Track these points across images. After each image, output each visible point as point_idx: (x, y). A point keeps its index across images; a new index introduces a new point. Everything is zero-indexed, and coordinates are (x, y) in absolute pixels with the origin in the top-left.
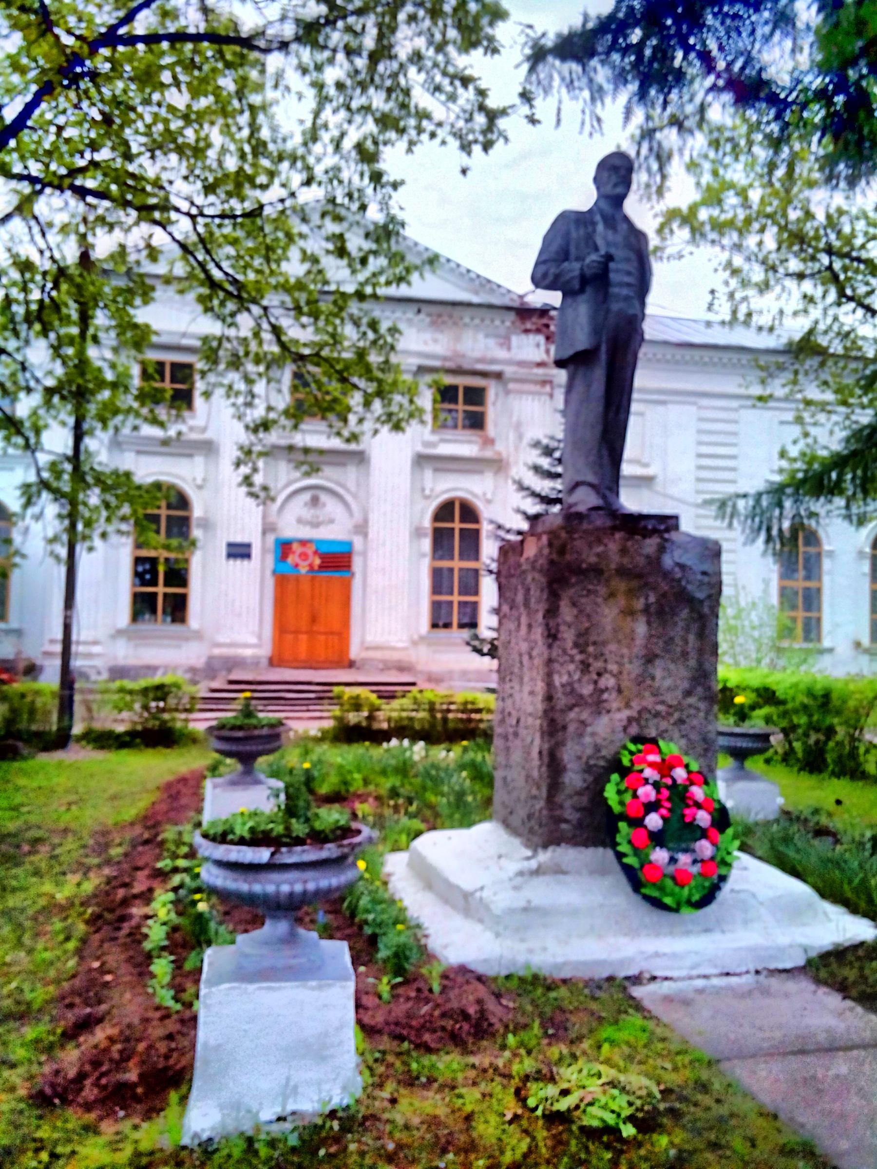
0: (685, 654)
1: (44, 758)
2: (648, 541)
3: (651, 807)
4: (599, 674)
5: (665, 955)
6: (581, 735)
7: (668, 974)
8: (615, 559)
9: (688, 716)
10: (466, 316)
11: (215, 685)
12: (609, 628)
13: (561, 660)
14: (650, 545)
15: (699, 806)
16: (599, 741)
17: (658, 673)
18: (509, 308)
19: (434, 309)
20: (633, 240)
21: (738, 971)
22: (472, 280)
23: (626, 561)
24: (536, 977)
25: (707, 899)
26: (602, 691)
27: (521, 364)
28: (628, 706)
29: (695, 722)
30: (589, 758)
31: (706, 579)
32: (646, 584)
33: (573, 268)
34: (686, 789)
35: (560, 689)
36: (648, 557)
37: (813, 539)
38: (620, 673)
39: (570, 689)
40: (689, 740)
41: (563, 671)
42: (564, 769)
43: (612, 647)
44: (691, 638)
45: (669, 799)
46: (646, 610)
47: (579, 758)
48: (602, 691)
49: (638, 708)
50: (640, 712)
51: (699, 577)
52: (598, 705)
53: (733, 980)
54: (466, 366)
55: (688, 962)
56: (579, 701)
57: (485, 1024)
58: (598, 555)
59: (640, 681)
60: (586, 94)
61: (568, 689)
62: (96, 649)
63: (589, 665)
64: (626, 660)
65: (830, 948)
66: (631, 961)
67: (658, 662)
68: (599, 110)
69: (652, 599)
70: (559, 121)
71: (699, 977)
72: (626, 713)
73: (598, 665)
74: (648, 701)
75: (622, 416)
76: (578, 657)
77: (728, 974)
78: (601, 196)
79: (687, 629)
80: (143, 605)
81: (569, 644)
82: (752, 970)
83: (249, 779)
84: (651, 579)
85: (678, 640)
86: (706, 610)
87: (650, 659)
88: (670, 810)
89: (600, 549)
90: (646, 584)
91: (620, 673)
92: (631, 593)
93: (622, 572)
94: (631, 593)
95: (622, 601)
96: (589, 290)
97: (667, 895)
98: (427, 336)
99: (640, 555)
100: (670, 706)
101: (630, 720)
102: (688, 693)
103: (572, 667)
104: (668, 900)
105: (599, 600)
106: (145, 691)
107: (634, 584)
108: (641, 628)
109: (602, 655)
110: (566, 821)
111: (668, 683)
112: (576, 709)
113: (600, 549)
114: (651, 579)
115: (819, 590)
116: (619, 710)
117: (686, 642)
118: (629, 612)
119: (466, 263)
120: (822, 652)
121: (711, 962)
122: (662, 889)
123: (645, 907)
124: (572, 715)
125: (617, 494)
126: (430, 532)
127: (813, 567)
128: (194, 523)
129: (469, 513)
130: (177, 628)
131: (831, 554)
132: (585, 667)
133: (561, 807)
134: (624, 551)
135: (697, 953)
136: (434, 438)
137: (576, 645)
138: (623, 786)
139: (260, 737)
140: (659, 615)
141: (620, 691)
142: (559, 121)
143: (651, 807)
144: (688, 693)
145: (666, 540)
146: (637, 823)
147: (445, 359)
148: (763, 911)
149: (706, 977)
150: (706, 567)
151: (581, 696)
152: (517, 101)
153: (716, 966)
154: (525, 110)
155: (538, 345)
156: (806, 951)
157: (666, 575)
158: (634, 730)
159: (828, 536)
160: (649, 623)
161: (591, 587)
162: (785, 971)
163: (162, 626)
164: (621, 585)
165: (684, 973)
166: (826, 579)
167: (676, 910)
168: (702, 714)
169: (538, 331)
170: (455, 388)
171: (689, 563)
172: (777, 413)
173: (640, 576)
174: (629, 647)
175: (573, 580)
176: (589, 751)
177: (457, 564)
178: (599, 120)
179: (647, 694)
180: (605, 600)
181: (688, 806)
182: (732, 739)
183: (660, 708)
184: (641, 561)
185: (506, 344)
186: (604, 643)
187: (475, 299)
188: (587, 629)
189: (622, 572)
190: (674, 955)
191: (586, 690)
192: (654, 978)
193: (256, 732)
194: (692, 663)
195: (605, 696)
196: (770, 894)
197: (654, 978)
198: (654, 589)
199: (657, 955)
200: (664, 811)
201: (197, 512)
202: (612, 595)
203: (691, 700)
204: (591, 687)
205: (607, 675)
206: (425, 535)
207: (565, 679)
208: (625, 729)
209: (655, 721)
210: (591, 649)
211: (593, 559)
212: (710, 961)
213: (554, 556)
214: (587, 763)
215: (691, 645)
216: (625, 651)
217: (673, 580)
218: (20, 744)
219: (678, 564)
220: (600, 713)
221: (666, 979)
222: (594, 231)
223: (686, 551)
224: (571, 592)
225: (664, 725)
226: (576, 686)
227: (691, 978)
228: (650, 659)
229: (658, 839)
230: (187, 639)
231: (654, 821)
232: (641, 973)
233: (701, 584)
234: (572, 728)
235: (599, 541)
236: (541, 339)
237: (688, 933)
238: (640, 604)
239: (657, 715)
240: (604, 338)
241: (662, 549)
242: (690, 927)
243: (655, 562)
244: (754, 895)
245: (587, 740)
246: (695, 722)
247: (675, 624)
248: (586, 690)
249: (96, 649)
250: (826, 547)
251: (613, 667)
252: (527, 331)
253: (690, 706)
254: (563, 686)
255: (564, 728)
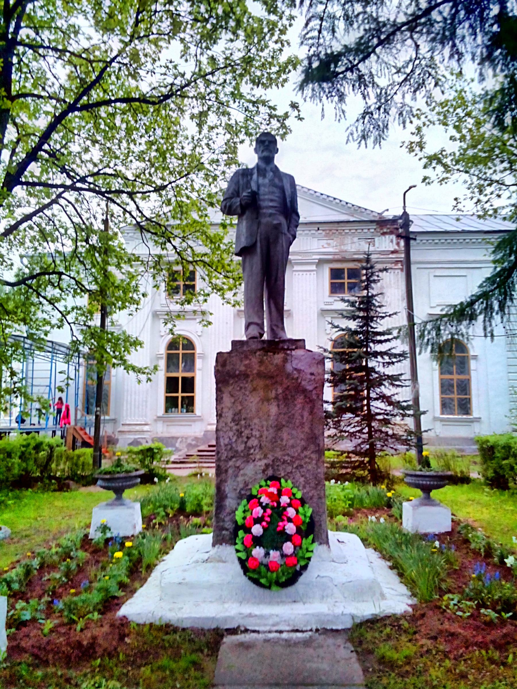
0: (302, 424)
1: (84, 490)
2: (276, 356)
3: (258, 521)
4: (248, 438)
5: (256, 616)
6: (236, 476)
7: (257, 628)
8: (256, 368)
9: (306, 463)
10: (346, 228)
11: (201, 448)
12: (254, 409)
13: (224, 429)
14: (278, 358)
15: (290, 520)
16: (247, 479)
17: (285, 436)
18: (372, 222)
19: (325, 227)
20: (276, 181)
21: (304, 629)
22: (350, 208)
23: (262, 369)
24: (168, 626)
25: (292, 579)
26: (250, 448)
27: (381, 253)
28: (265, 457)
29: (310, 467)
30: (242, 489)
31: (313, 377)
32: (276, 382)
33: (237, 201)
34: (285, 509)
35: (224, 448)
36: (277, 365)
37: (462, 347)
38: (261, 436)
39: (230, 447)
40: (306, 478)
41: (226, 437)
42: (226, 497)
43: (256, 421)
44: (306, 414)
45: (270, 516)
46: (276, 398)
47: (235, 490)
48: (250, 448)
49: (272, 458)
50: (273, 461)
51: (309, 376)
52: (247, 457)
53: (299, 635)
54: (348, 257)
55: (271, 622)
56: (235, 455)
57: (91, 651)
58: (246, 366)
59: (274, 440)
60: (336, 99)
61: (229, 447)
62: (146, 428)
63: (241, 433)
64: (265, 428)
65: (370, 617)
66: (232, 618)
67: (285, 429)
68: (344, 107)
69: (280, 391)
70: (323, 116)
71: (276, 631)
72: (264, 462)
73: (247, 432)
74: (279, 454)
75: (279, 283)
76: (235, 428)
77: (297, 631)
78: (259, 158)
79: (303, 408)
80: (171, 403)
81: (229, 420)
82: (314, 628)
83: (117, 503)
84: (278, 379)
85: (297, 416)
86: (314, 397)
87: (279, 428)
88: (268, 523)
89: (247, 362)
90: (276, 382)
91: (261, 436)
92: (267, 388)
93: (260, 375)
94: (267, 388)
95: (261, 393)
96: (247, 213)
97: (263, 578)
98: (324, 242)
99: (272, 364)
100: (293, 457)
101: (267, 466)
102: (305, 449)
103: (231, 434)
104: (263, 581)
105: (247, 393)
106: (142, 452)
107: (268, 382)
108: (273, 409)
109: (249, 426)
110: (227, 530)
111: (291, 442)
112: (234, 459)
113: (247, 362)
114: (278, 379)
115: (469, 380)
116: (260, 459)
117: (302, 416)
118: (266, 400)
119: (345, 199)
120: (472, 421)
121: (286, 622)
122: (259, 573)
123: (249, 583)
124: (231, 463)
125: (283, 329)
126: (164, 356)
127: (463, 365)
128: (197, 356)
129: (190, 345)
130: (190, 414)
131: (475, 357)
132: (240, 434)
133: (224, 521)
134: (261, 362)
135: (277, 616)
136: (331, 300)
137: (233, 420)
138: (247, 508)
139: (119, 478)
140: (286, 400)
141: (261, 447)
142: (323, 116)
143: (258, 521)
144: (305, 449)
145: (288, 355)
146: (248, 530)
147: (335, 254)
148: (335, 590)
149: (281, 632)
150: (313, 370)
151: (237, 451)
152: (289, 109)
153: (289, 625)
154: (296, 113)
155: (392, 241)
156: (353, 618)
157: (288, 376)
158: (270, 472)
159: (473, 347)
160: (278, 406)
161: (241, 385)
162: (337, 631)
163: (179, 414)
164: (261, 383)
165: (267, 628)
166: (473, 374)
167: (269, 587)
168: (314, 462)
169: (391, 233)
170: (342, 271)
171: (302, 368)
172: (433, 270)
173: (272, 377)
174: (267, 420)
175: (231, 382)
176: (241, 486)
177: (180, 374)
178: (343, 112)
179: (278, 449)
180: (251, 392)
181: (283, 520)
182: (414, 478)
183: (286, 458)
184: (272, 368)
185: (371, 241)
186: (251, 419)
187: (352, 219)
188: (240, 410)
189: (260, 375)
190: (261, 617)
191: (241, 447)
192: (246, 631)
193: (117, 476)
194: (306, 429)
195: (252, 451)
196: (344, 579)
197: (246, 631)
198: (281, 384)
199: (250, 615)
200: (264, 523)
201: (198, 350)
202: (255, 389)
203: (307, 453)
204: (243, 446)
205: (253, 438)
206: (162, 358)
207: (227, 441)
208: (264, 471)
209: (284, 466)
210: (243, 422)
211: (243, 368)
212: (285, 621)
213: (220, 368)
214: (240, 492)
215: (305, 418)
216: (265, 423)
217: (293, 379)
218: (71, 482)
219: (296, 369)
220: (248, 462)
221: (254, 631)
222: (251, 179)
223: (300, 360)
224: (230, 388)
225: (289, 469)
226: (234, 445)
227: (270, 632)
228: (279, 428)
229: (257, 541)
230: (194, 421)
231: (257, 530)
232: (239, 627)
233: (310, 380)
234: (230, 471)
235: (246, 357)
236: (393, 237)
237: (282, 602)
238: (273, 394)
239: (284, 462)
240: (258, 239)
241: (285, 360)
242: (284, 599)
243: (281, 369)
244: (331, 580)
245: (240, 479)
246: (310, 467)
247: (295, 405)
248: (241, 447)
249: (146, 428)
250: (472, 353)
251: (256, 433)
252: (384, 234)
253: (306, 457)
254: (226, 445)
255: (226, 471)
